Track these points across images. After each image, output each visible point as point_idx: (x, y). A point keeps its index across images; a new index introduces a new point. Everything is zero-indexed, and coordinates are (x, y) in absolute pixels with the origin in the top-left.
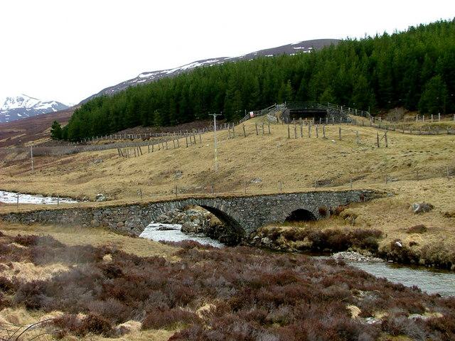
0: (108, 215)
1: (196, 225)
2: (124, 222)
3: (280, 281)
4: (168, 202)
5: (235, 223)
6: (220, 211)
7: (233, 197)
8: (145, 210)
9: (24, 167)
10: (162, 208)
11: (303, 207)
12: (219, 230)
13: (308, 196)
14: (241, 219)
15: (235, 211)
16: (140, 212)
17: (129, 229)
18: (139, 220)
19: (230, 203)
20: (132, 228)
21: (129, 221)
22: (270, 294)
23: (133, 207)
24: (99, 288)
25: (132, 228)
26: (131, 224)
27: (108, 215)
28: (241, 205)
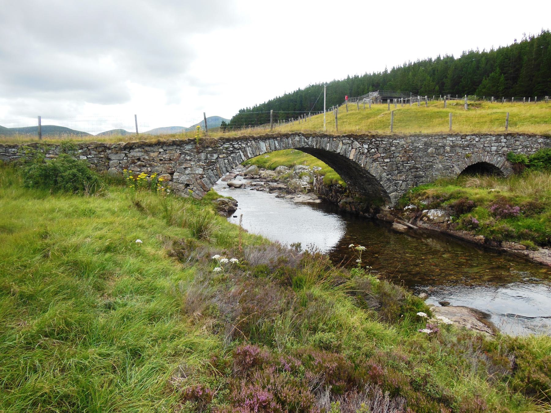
0: (139, 159)
1: (305, 183)
2: (172, 174)
3: (509, 261)
4: (254, 139)
5: (372, 180)
6: (348, 159)
7: (373, 136)
8: (212, 153)
9: (294, 324)
10: (245, 151)
11: (487, 159)
12: (337, 191)
13: (497, 141)
14: (385, 174)
15: (375, 160)
16: (203, 156)
17: (182, 186)
18: (200, 171)
19: (366, 146)
20: (187, 185)
21: (182, 173)
22: (466, 270)
23: (188, 147)
24: (298, 322)
25: (187, 185)
26: (184, 178)
27: (139, 159)
28: (386, 150)
